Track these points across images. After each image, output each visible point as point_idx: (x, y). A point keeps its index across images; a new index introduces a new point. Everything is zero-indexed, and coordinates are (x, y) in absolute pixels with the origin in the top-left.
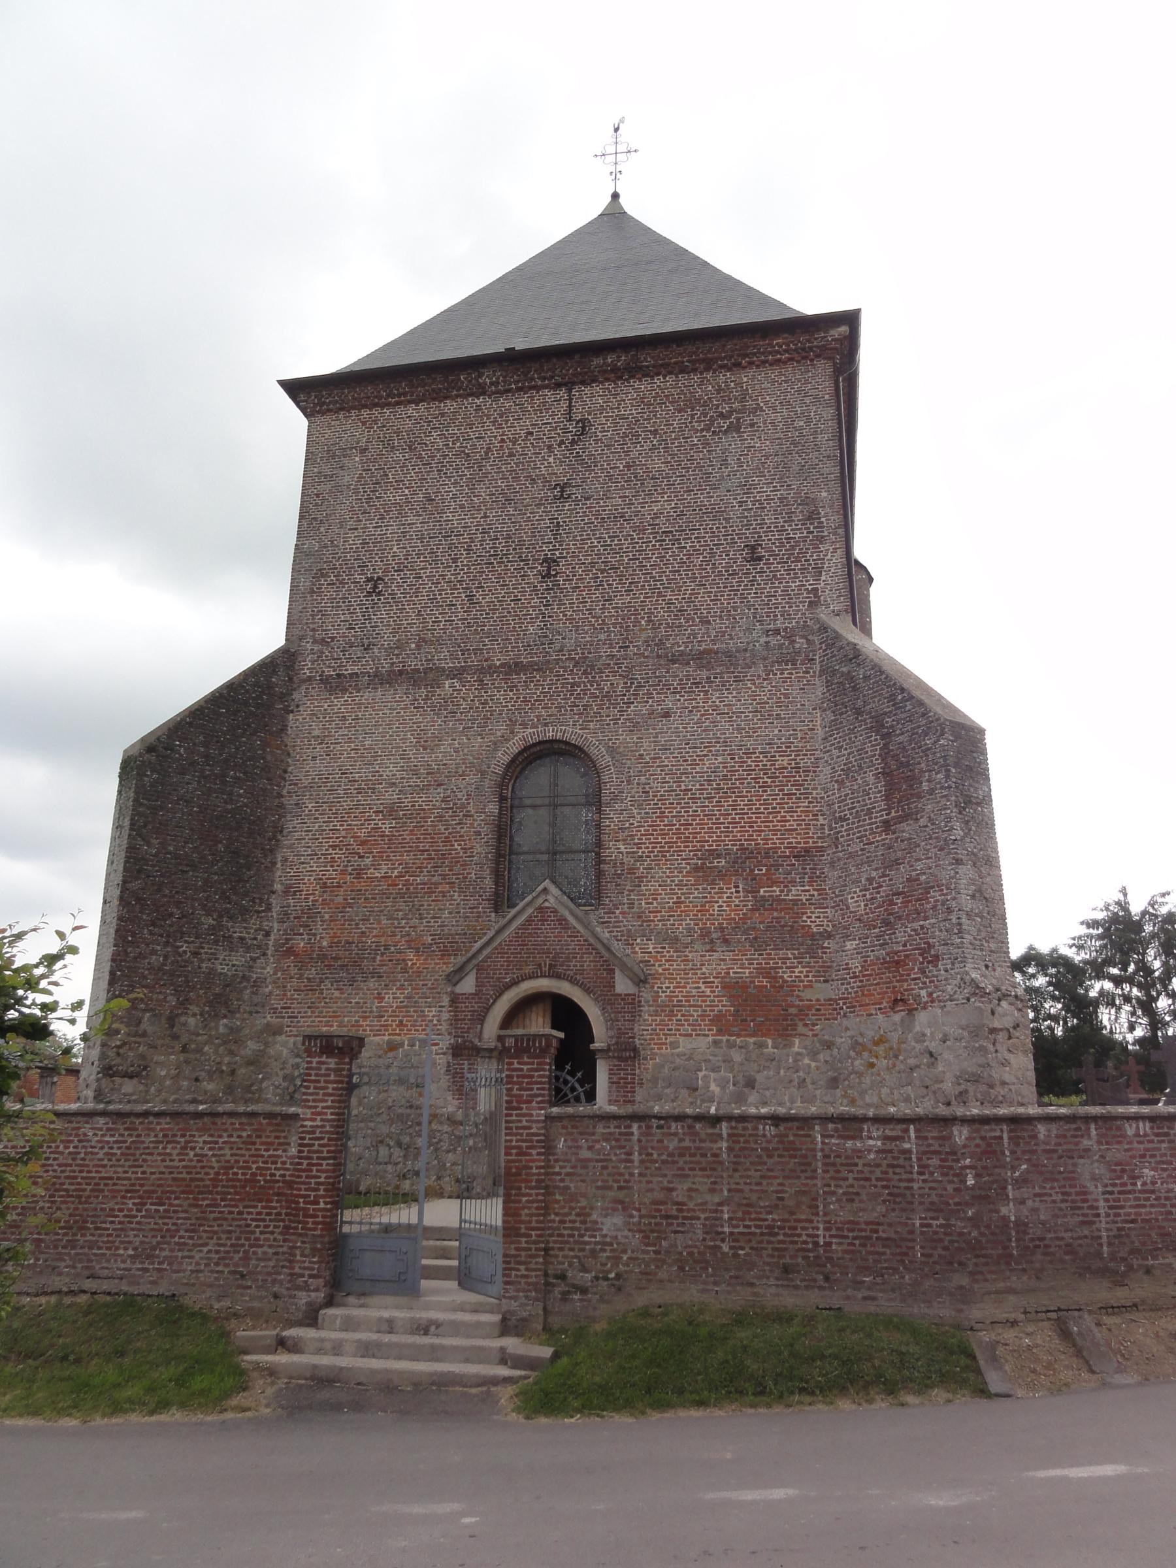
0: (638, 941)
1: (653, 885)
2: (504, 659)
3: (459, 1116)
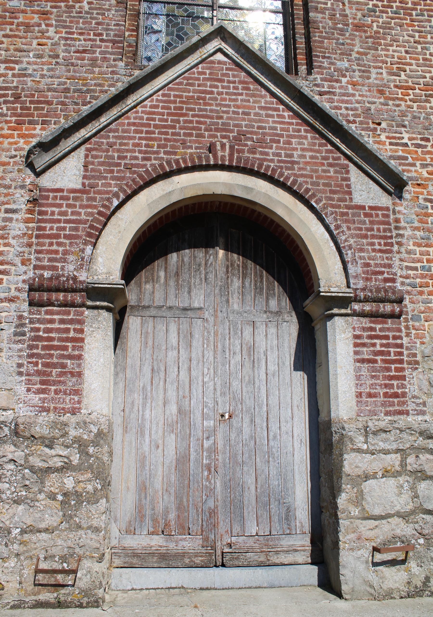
0: (384, 125)
1: (396, 52)
2: (359, 553)
3: (42, 425)
